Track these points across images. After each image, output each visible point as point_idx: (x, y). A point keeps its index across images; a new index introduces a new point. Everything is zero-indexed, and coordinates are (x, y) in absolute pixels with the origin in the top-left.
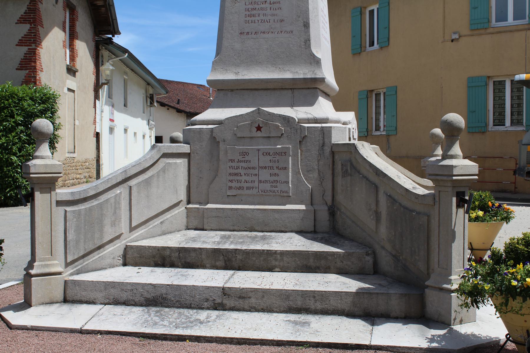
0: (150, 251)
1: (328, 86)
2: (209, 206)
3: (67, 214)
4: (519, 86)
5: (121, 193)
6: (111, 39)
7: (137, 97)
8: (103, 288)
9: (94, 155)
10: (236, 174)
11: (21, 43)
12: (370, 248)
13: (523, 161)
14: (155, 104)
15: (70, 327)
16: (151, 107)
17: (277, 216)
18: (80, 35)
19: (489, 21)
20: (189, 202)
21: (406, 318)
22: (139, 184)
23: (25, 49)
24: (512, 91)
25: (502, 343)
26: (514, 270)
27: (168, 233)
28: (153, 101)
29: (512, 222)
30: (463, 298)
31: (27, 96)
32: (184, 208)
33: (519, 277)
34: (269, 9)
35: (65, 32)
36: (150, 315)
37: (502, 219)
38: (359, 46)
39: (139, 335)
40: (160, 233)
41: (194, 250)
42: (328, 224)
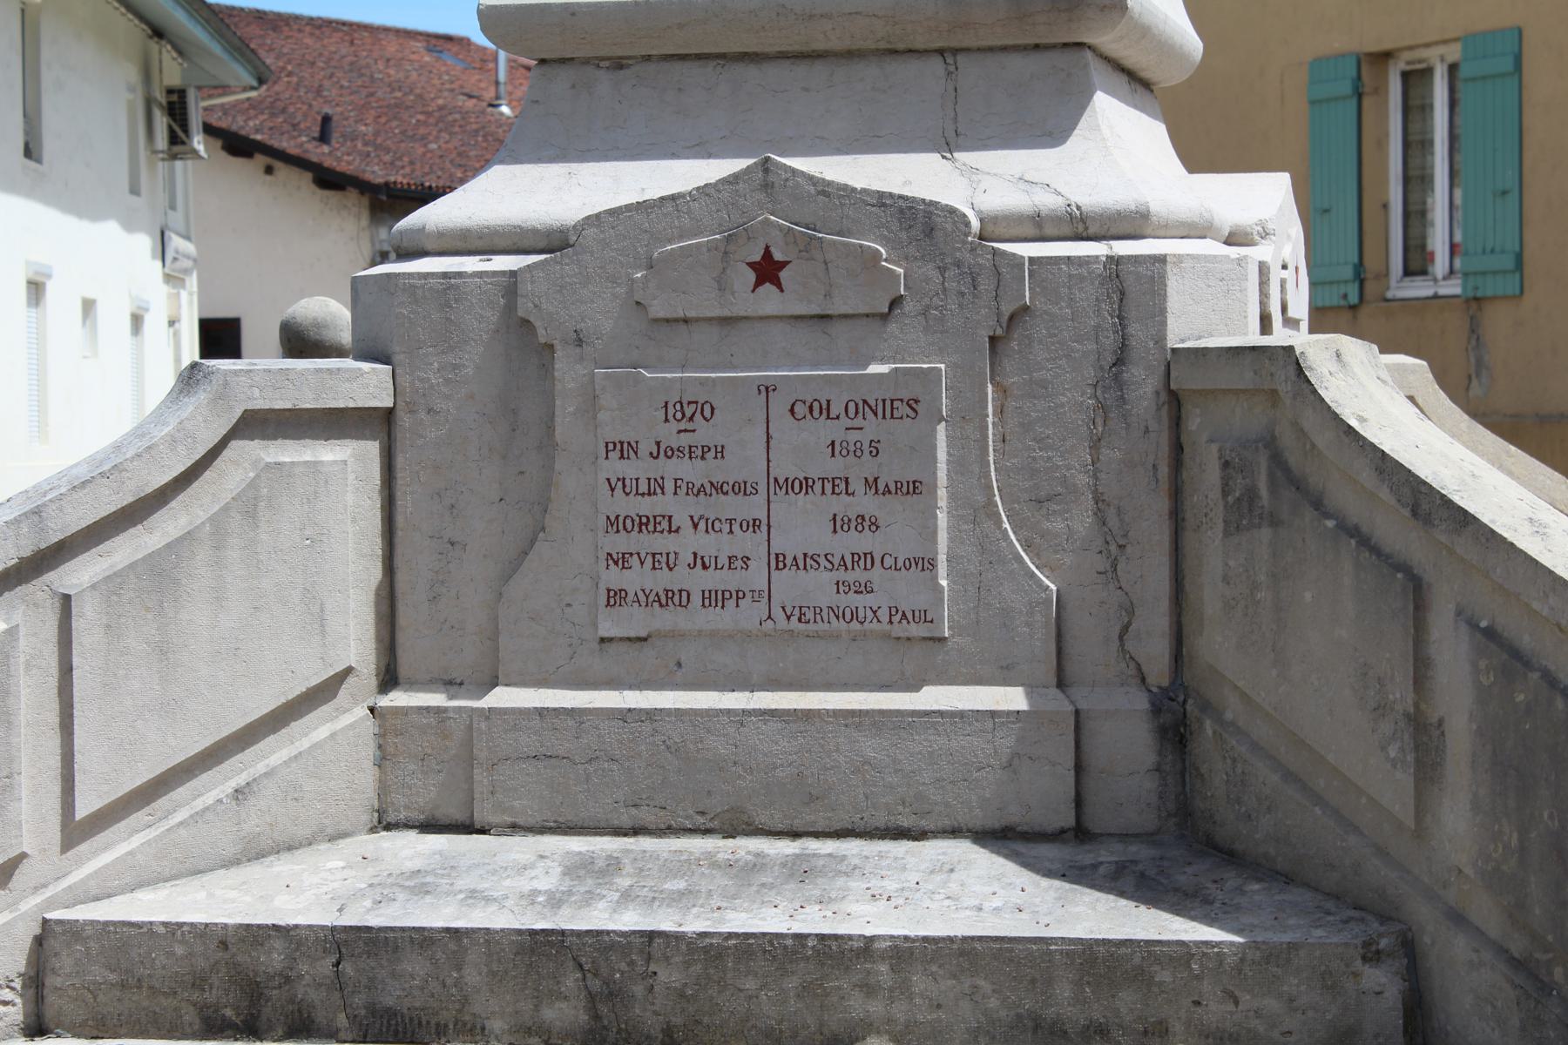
0: (180, 950)
2: (503, 697)
10: (643, 524)
12: (1384, 918)
14: (198, 142)
16: (174, 157)
20: (389, 679)
22: (111, 585)
28: (186, 131)
32: (361, 711)
40: (230, 851)
41: (422, 939)
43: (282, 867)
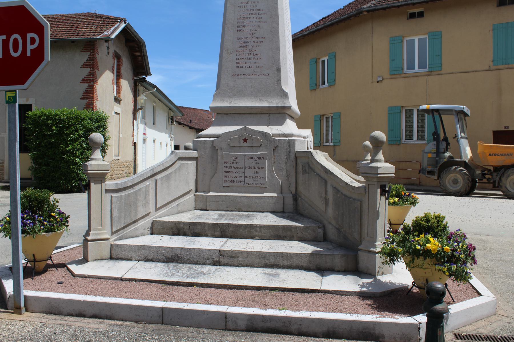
1: (293, 112)
2: (211, 194)
3: (113, 198)
4: (422, 113)
6: (145, 78)
7: (162, 118)
8: (137, 250)
9: (131, 158)
10: (229, 172)
11: (84, 81)
12: (321, 223)
13: (425, 164)
14: (175, 123)
17: (257, 201)
18: (123, 76)
19: (402, 69)
20: (196, 191)
21: (345, 271)
22: (162, 178)
23: (86, 85)
24: (418, 117)
25: (409, 288)
26: (418, 238)
29: (417, 205)
30: (384, 257)
31: (87, 117)
32: (193, 195)
33: (421, 243)
34: (253, 59)
35: (114, 74)
36: (169, 269)
37: (411, 204)
38: (315, 85)
40: (176, 212)
41: (200, 224)
42: (292, 206)
43: (183, 214)
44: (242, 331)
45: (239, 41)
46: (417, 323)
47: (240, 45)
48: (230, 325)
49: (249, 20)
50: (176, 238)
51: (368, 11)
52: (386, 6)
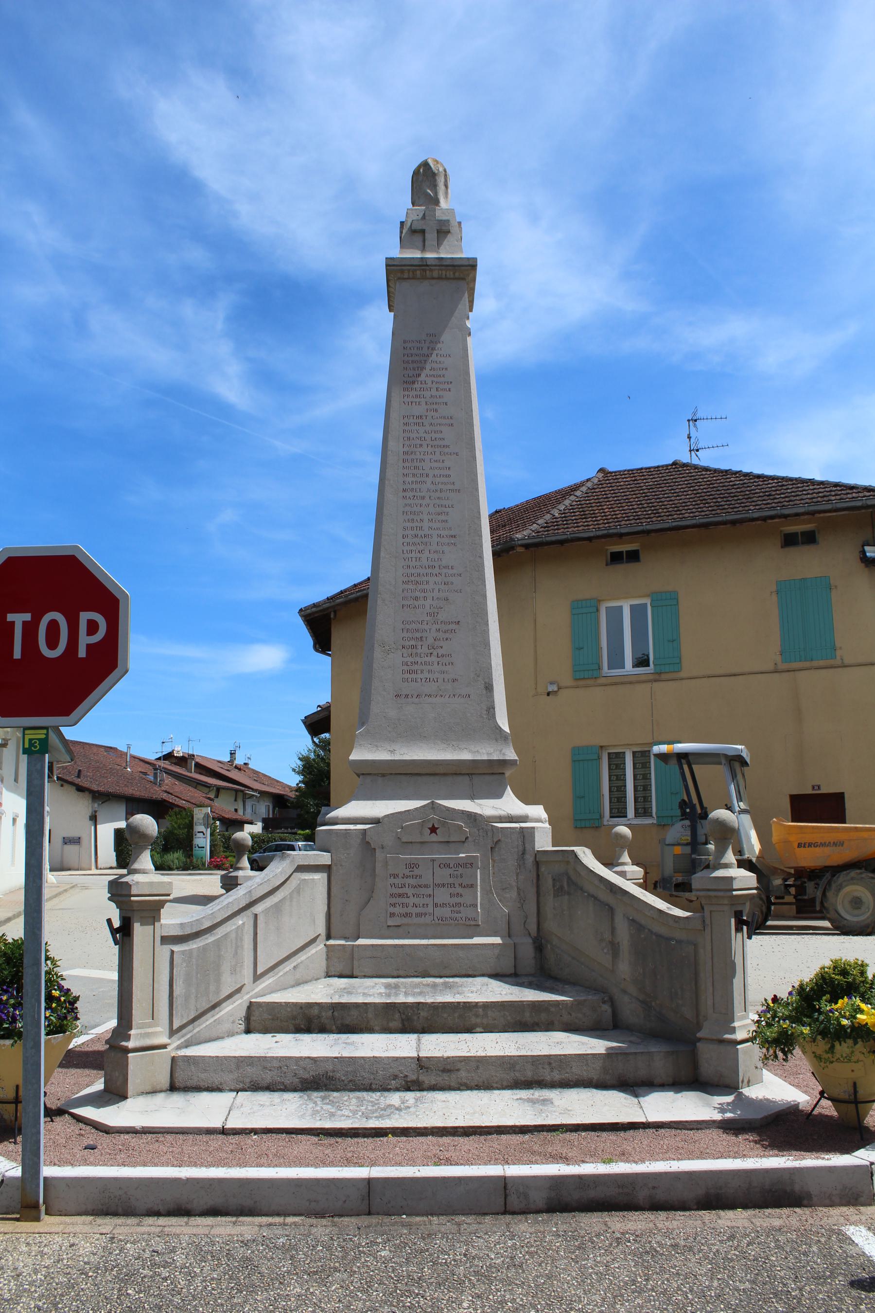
0: (289, 1010)
2: (361, 942)
5: (243, 924)
10: (400, 895)
12: (604, 993)
15: (205, 1126)
19: (600, 668)
20: (329, 937)
22: (267, 911)
27: (303, 983)
32: (322, 946)
39: (315, 1132)
40: (292, 983)
41: (357, 1005)
42: (535, 962)
43: (307, 987)
44: (538, 1212)
45: (407, 626)
46: (868, 1163)
47: (410, 635)
48: (514, 1202)
49: (426, 587)
50: (306, 1038)
51: (527, 546)
52: (565, 537)
